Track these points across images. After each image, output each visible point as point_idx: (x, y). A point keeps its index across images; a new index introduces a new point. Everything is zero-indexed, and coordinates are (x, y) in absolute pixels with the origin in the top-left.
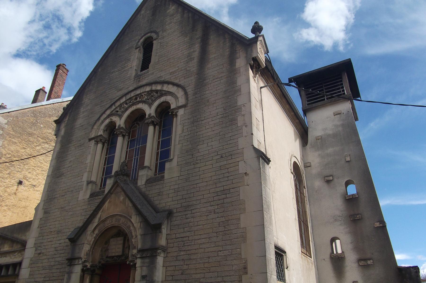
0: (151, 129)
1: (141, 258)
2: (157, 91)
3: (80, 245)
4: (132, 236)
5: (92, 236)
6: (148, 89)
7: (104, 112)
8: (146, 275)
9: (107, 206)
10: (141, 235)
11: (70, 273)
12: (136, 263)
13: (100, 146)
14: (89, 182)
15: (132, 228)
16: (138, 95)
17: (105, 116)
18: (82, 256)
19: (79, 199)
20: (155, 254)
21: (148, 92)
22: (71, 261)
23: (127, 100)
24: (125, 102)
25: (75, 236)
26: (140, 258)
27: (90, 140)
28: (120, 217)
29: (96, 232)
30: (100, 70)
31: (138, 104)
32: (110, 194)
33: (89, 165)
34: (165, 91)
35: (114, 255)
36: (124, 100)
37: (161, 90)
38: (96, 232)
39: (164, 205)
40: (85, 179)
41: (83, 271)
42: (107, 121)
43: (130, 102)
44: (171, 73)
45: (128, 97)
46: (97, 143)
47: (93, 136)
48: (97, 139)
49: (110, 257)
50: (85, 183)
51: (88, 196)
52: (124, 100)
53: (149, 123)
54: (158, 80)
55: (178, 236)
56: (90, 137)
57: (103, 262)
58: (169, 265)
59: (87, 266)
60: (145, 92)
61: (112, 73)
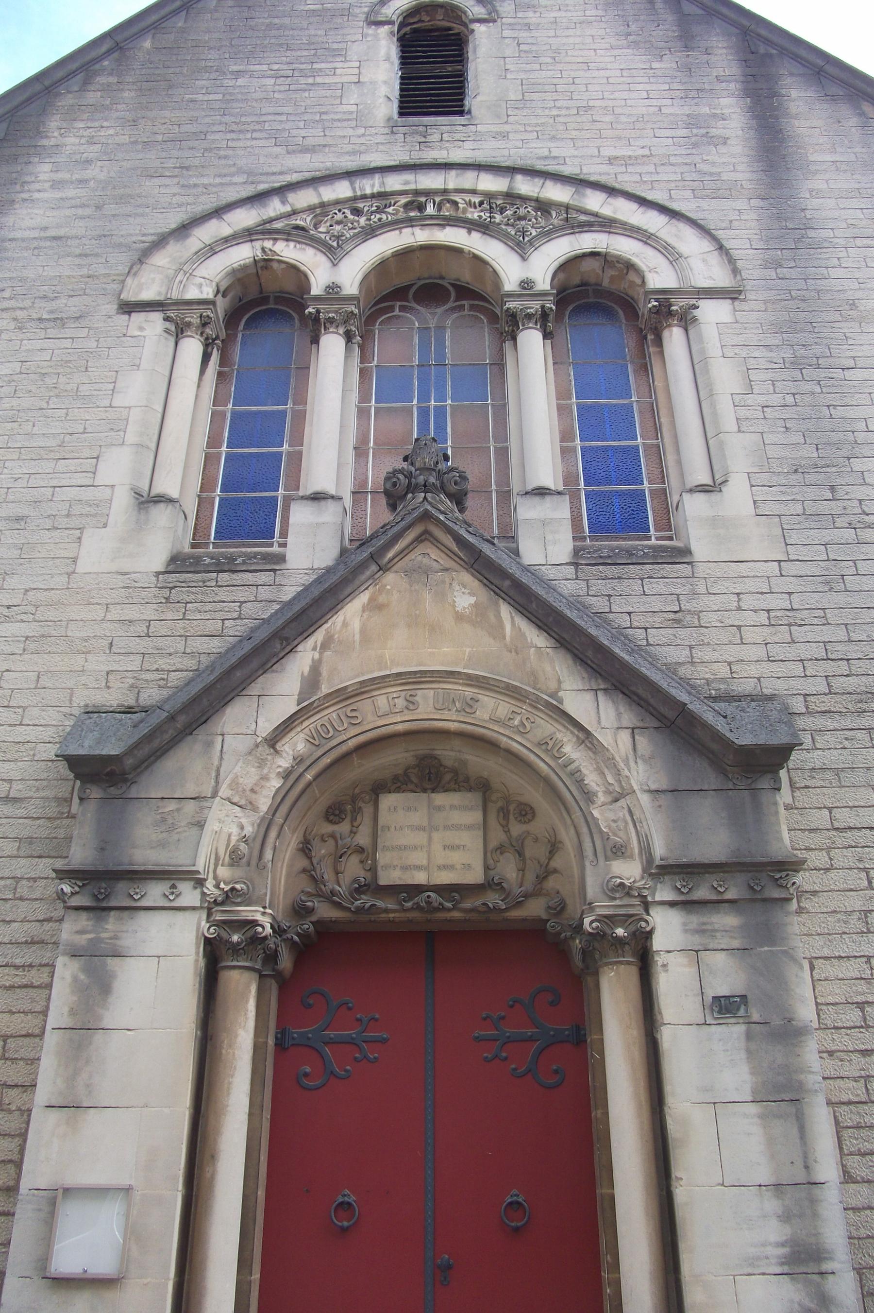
0: (532, 342)
1: (687, 905)
2: (543, 207)
3: (172, 806)
4: (589, 796)
5: (261, 763)
6: (489, 183)
7: (218, 212)
8: (744, 997)
9: (356, 625)
10: (655, 793)
11: (98, 966)
12: (649, 934)
13: (192, 348)
14: (148, 500)
15: (571, 750)
16: (428, 193)
17: (245, 218)
18: (200, 866)
19: (81, 567)
20: (776, 894)
21: (490, 196)
22: (105, 887)
23: (364, 197)
24: (354, 205)
25: (131, 751)
26: (672, 904)
27: (129, 308)
28: (469, 692)
29: (296, 744)
30: (147, 44)
31: (443, 226)
32: (374, 568)
33: (135, 415)
34: (586, 212)
35: (420, 878)
36: (342, 190)
37: (567, 207)
38: (296, 744)
39: (723, 671)
40: (118, 471)
41: (215, 956)
42: (243, 254)
43: (379, 210)
44: (611, 160)
45: (370, 185)
46: (179, 331)
47: (147, 295)
48: (177, 316)
49: (393, 890)
50: (122, 501)
51: (157, 560)
52: (342, 190)
53: (529, 316)
54: (540, 166)
55: (844, 817)
56: (130, 295)
57: (325, 911)
58: (826, 952)
59: (254, 923)
60: (474, 192)
61: (238, 74)
